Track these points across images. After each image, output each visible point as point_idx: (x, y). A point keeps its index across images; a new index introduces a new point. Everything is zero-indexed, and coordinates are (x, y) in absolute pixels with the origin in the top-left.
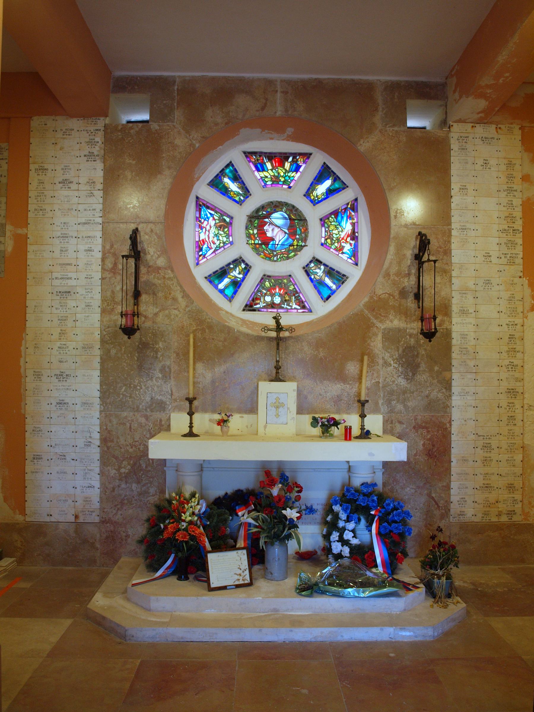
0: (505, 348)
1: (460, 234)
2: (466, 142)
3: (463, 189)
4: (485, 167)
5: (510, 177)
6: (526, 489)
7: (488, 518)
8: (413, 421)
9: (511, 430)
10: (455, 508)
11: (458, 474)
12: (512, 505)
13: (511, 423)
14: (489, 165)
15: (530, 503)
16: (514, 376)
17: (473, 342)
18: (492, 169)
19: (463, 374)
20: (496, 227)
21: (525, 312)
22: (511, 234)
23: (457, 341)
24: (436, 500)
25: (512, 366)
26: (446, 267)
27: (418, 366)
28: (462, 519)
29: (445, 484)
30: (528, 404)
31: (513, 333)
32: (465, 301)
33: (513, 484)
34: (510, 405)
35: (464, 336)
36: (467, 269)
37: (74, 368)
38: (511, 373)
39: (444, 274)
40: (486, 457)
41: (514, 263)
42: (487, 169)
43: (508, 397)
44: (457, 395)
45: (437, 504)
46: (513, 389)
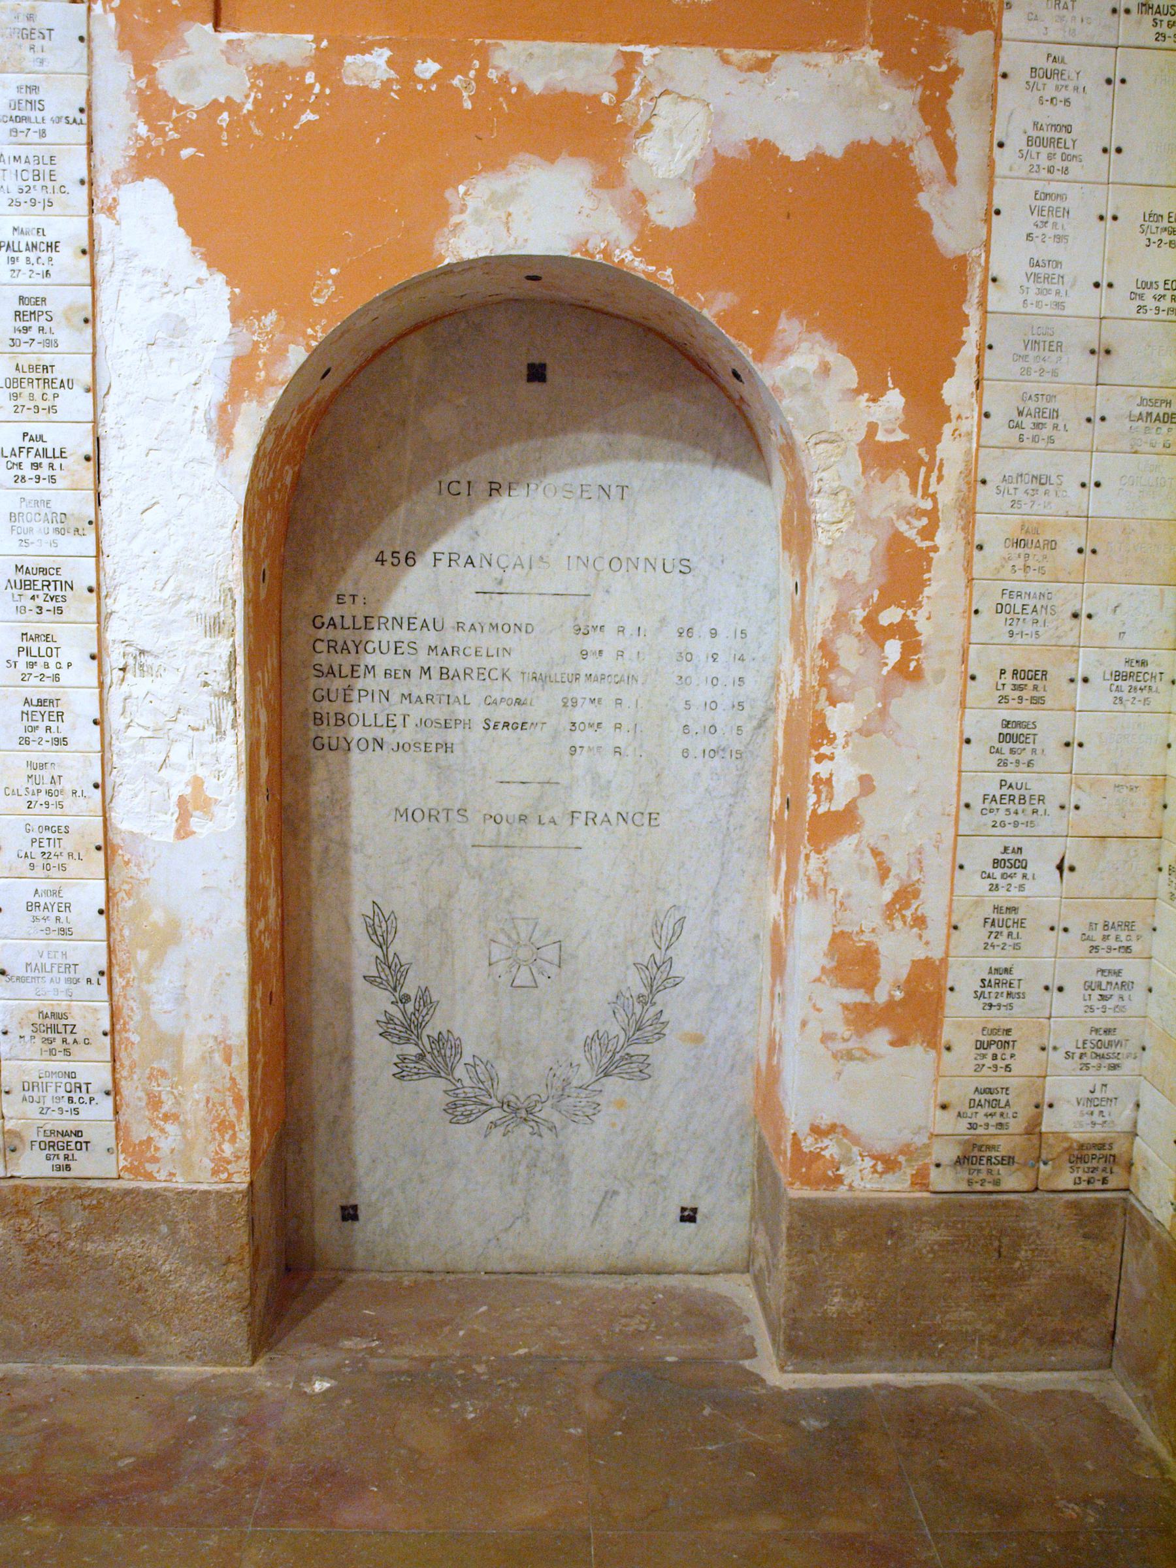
6: (135, 1038)
9: (43, 766)
12: (65, 1105)
13: (41, 732)
15: (154, 1102)
33: (64, 1016)
34: (34, 646)
38: (30, 490)
43: (22, 610)
46: (43, 571)
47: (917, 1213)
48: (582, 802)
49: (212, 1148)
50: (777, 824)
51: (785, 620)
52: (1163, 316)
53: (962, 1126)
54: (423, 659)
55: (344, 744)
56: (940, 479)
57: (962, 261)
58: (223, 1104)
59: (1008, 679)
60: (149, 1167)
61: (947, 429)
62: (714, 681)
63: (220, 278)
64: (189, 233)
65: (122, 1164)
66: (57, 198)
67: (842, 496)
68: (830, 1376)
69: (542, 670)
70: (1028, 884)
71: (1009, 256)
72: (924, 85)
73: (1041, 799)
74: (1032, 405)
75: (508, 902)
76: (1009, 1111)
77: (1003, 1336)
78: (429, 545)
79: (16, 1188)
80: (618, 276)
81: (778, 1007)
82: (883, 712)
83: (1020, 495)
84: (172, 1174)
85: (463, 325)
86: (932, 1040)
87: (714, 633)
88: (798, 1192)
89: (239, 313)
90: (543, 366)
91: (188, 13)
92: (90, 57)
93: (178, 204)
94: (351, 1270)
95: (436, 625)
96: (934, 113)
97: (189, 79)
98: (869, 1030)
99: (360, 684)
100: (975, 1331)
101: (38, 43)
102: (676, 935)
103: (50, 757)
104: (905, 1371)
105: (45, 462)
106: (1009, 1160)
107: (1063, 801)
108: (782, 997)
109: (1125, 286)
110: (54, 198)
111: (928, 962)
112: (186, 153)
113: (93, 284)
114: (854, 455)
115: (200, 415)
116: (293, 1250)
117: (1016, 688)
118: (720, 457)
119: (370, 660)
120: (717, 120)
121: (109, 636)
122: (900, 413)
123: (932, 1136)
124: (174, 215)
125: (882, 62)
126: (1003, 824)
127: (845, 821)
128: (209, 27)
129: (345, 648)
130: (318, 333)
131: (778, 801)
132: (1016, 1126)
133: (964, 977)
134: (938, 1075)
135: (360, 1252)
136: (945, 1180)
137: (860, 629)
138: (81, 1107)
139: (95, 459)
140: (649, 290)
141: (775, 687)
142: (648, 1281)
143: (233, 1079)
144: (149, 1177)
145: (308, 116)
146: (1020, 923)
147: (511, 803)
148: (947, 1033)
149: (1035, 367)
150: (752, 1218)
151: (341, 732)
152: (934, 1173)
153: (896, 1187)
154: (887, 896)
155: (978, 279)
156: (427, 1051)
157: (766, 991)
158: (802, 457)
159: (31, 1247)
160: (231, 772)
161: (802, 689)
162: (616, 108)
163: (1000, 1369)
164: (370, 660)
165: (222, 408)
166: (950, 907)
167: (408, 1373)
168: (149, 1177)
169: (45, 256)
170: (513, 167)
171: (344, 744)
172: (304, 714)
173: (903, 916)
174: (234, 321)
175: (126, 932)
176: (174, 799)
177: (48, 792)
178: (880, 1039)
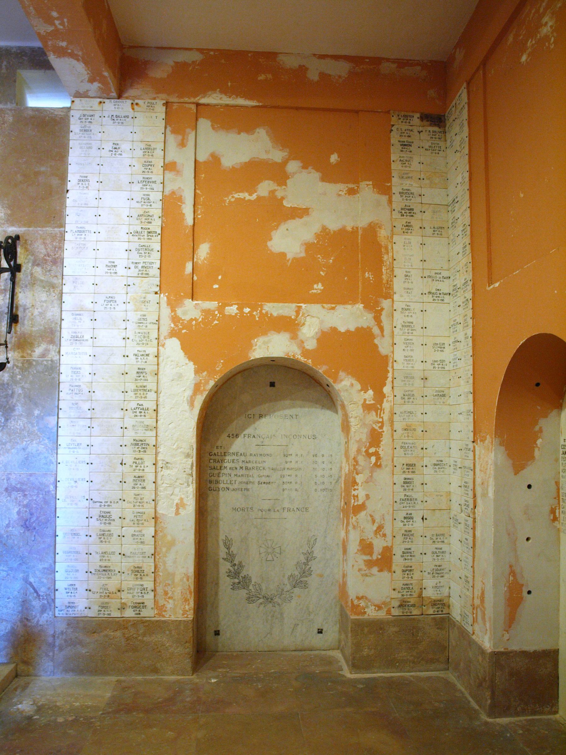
0: (131, 386)
1: (76, 238)
2: (90, 122)
3: (84, 180)
4: (114, 153)
5: (148, 165)
6: (161, 574)
7: (106, 613)
8: (5, 481)
9: (138, 495)
10: (61, 598)
11: (64, 552)
12: (140, 595)
13: (138, 485)
14: (120, 150)
15: (166, 593)
16: (143, 422)
17: (88, 378)
18: (124, 155)
19: (75, 420)
20: (125, 229)
21: (162, 338)
22: (146, 237)
23: (67, 376)
24: (35, 586)
25: (141, 410)
26: (55, 281)
27: (12, 409)
28: (71, 612)
29: (46, 565)
30: (163, 460)
31: (143, 367)
32: (79, 324)
33: (141, 568)
34: (138, 461)
35: (76, 370)
36: (83, 283)
37: (89, 416)
38: (139, 419)
39: (52, 290)
40: (104, 531)
41: (147, 274)
42: (117, 156)
43: (134, 451)
44: (65, 448)
45: (36, 592)
46: (141, 441)
47: (388, 623)
48: (286, 505)
49: (182, 607)
50: (343, 510)
51: (343, 452)
52: (440, 369)
53: (399, 596)
54: (241, 464)
55: (217, 489)
56: (384, 413)
57: (387, 356)
58: (186, 593)
59: (405, 466)
60: (164, 613)
61: (385, 400)
62: (323, 469)
63: (192, 363)
64: (184, 352)
65: (156, 612)
66: (149, 343)
67: (358, 418)
68: (365, 675)
69: (275, 467)
70: (414, 524)
71: (399, 355)
72: (375, 312)
73: (416, 500)
74: (407, 393)
75: (265, 535)
76: (413, 591)
77: (416, 660)
78: (242, 433)
79: (124, 621)
80: (297, 362)
81: (345, 563)
82: (371, 476)
83: (405, 417)
84: (170, 615)
85: (252, 372)
86: (390, 570)
87: (323, 456)
88: (353, 617)
89: (197, 372)
90: (274, 383)
91: (186, 297)
92: (159, 308)
93: (181, 344)
94: (217, 652)
95: (244, 455)
96: (378, 319)
97: (185, 313)
98: (371, 568)
99: (222, 472)
100: (408, 659)
101: (146, 304)
102: (314, 544)
103: (141, 492)
104: (387, 673)
105: (143, 411)
106: (414, 605)
107: (422, 500)
108: (346, 560)
109: (429, 362)
110: (149, 343)
111: (387, 547)
112: (184, 331)
113: (158, 365)
114: (360, 407)
115: (185, 399)
116: (203, 643)
117: (407, 469)
118: (323, 407)
119: (225, 465)
120: (322, 322)
121: (158, 458)
122: (372, 396)
123: (391, 599)
124: (180, 347)
125: (364, 307)
126: (406, 507)
127: (362, 507)
128: (191, 300)
129: (218, 461)
130: (217, 377)
131: (343, 503)
132: (415, 595)
133: (398, 551)
134: (392, 580)
135: (220, 645)
136: (396, 612)
137: (364, 454)
138: (145, 595)
139: (156, 411)
140: (305, 365)
141: (341, 470)
142: (308, 652)
143: (189, 586)
144: (164, 616)
145: (216, 322)
146: (412, 535)
147: (266, 505)
148: (394, 568)
149: (407, 383)
150: (340, 632)
151: (217, 485)
152: (392, 610)
153: (382, 615)
154: (375, 528)
155: (391, 361)
156: (241, 580)
157: (341, 560)
158: (347, 408)
159: (127, 639)
160: (191, 496)
161: (349, 470)
162: (296, 320)
163: (416, 671)
164: (225, 465)
165: (191, 397)
166: (393, 531)
167: (239, 677)
168: (164, 616)
169: (145, 357)
170: (269, 335)
171: (217, 489)
172: (207, 480)
173: (380, 534)
174: (195, 374)
175: (160, 543)
176: (175, 504)
177: (140, 502)
178: (375, 570)
